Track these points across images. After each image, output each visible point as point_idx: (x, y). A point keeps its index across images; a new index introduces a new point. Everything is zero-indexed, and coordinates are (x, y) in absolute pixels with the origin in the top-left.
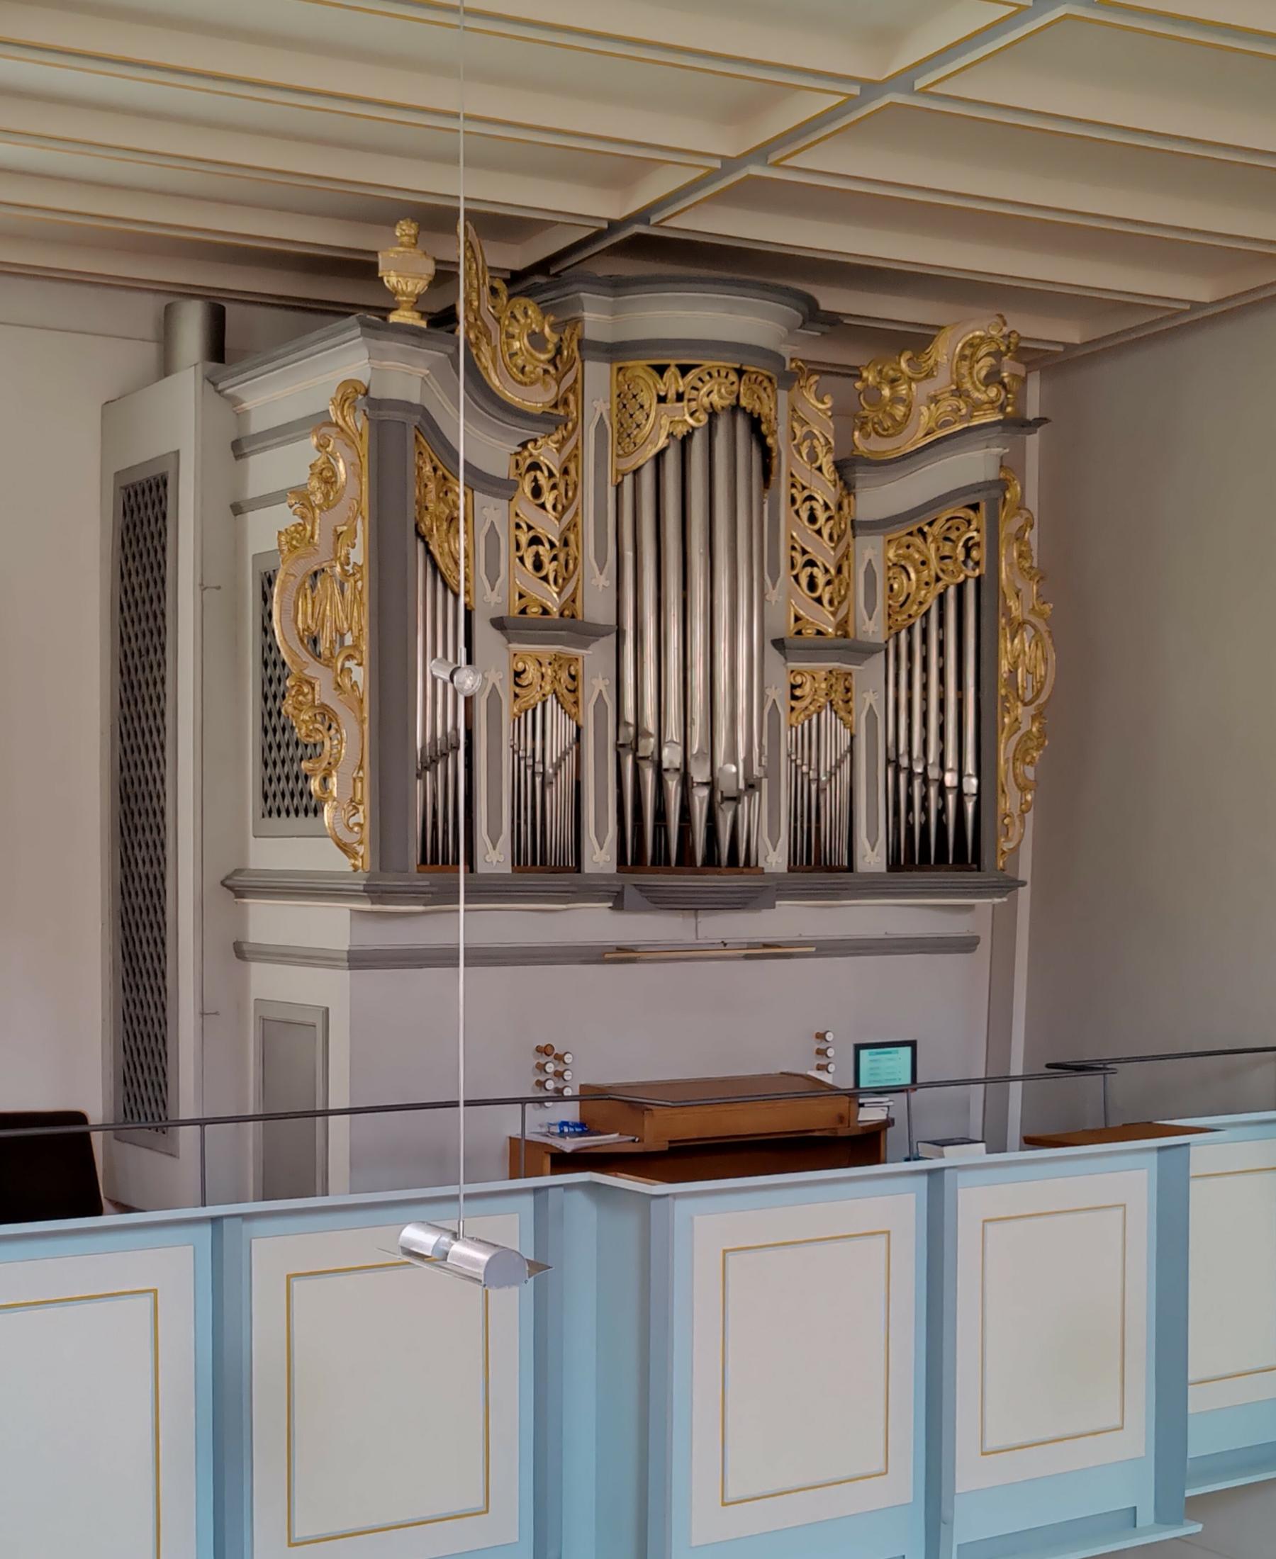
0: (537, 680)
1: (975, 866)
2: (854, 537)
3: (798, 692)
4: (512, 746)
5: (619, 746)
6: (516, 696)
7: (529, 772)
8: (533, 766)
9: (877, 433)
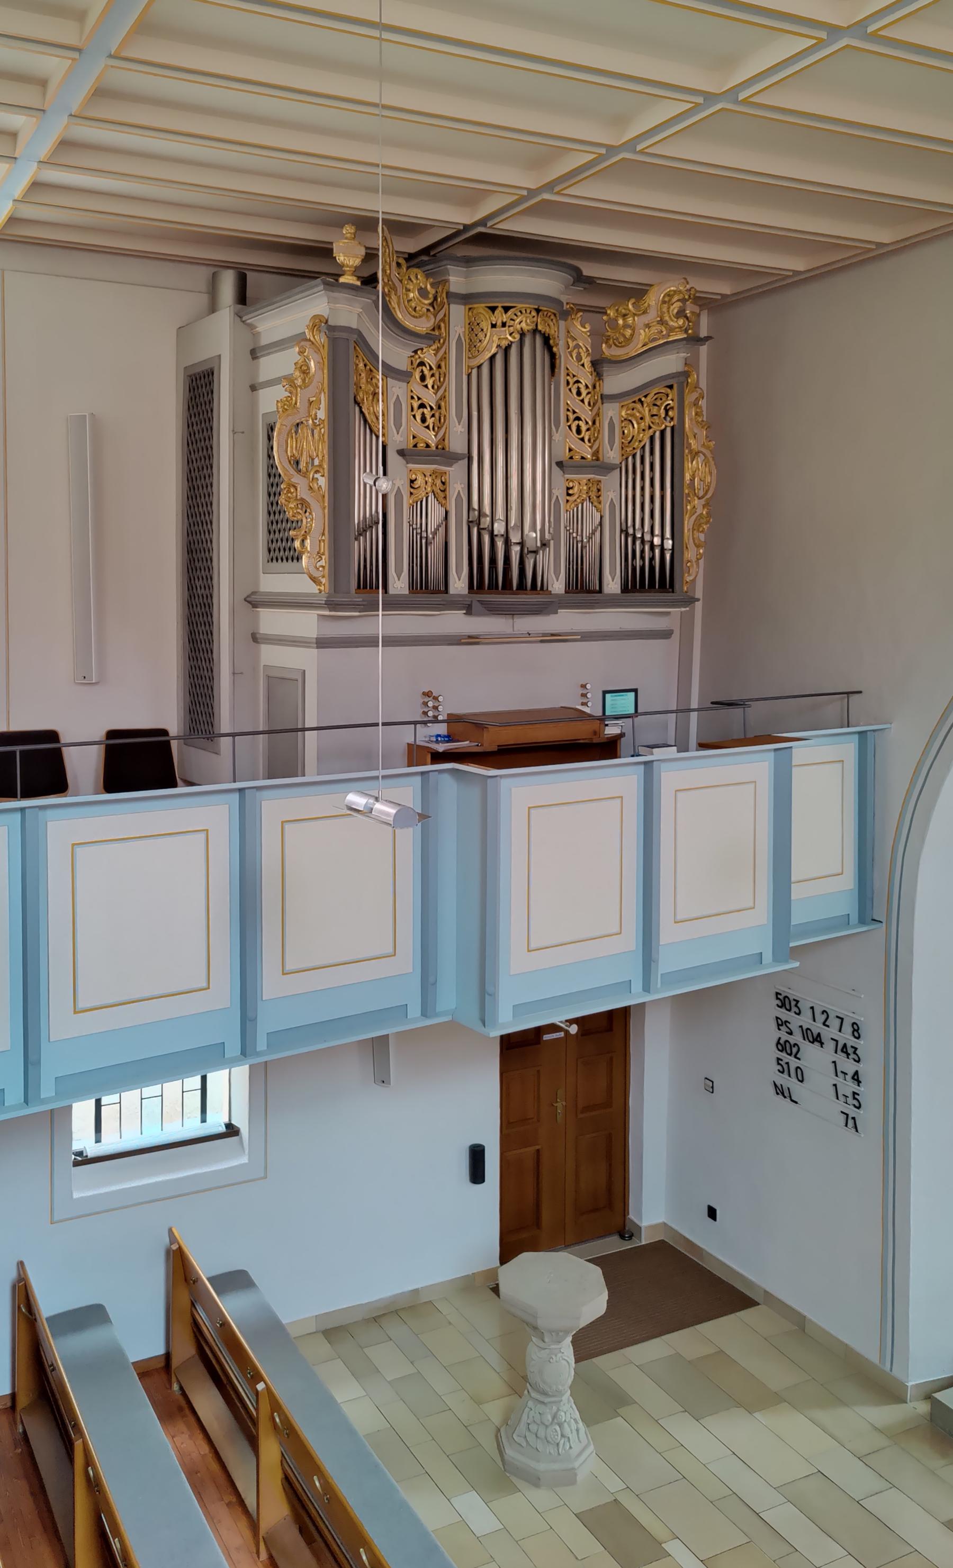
0: (423, 485)
1: (671, 590)
2: (602, 404)
3: (571, 492)
4: (409, 522)
5: (469, 522)
6: (411, 493)
7: (419, 537)
8: (421, 533)
9: (615, 345)
